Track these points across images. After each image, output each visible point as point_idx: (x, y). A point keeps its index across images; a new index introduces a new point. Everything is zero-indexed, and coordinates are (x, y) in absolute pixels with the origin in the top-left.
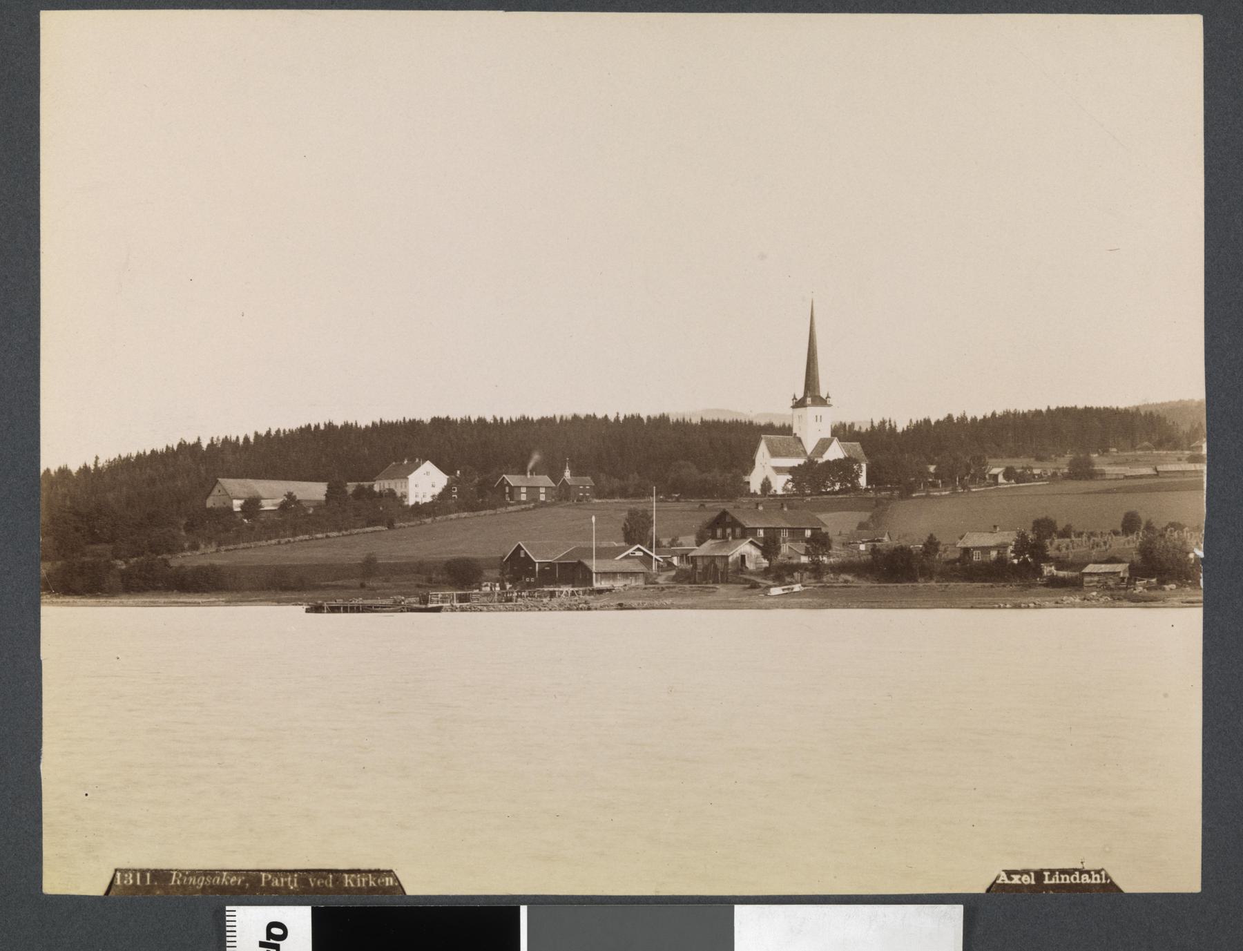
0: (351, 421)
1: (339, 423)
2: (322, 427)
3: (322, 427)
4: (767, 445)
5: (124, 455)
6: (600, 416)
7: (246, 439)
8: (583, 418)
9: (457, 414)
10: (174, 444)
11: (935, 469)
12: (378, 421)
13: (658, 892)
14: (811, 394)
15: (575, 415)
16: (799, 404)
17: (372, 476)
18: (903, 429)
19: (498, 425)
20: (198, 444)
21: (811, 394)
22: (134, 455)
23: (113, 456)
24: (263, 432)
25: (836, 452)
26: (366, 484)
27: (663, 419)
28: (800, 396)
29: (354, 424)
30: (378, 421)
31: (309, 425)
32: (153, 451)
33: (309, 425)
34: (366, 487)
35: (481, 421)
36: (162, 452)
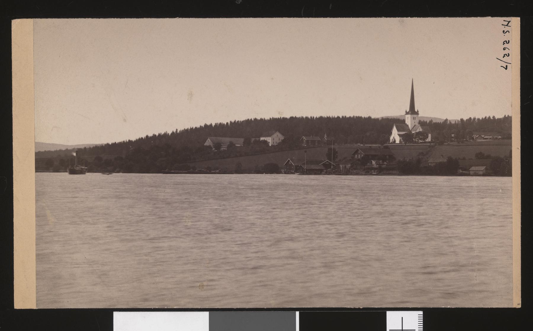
0: (263, 118)
1: (259, 118)
2: (253, 119)
3: (253, 119)
4: (396, 126)
5: (186, 128)
6: (304, 117)
7: (227, 123)
8: (496, 118)
9: (298, 115)
10: (203, 125)
11: (454, 135)
12: (272, 118)
13: (452, 295)
14: (412, 111)
15: (306, 117)
16: (407, 113)
17: (259, 137)
18: (505, 116)
19: (312, 119)
20: (211, 125)
21: (412, 111)
22: (189, 128)
23: (182, 129)
24: (233, 121)
25: (420, 129)
26: (257, 139)
27: (370, 118)
28: (408, 111)
29: (264, 119)
30: (272, 118)
31: (249, 119)
32: (196, 128)
33: (249, 119)
34: (258, 140)
35: (307, 118)
36: (199, 128)
